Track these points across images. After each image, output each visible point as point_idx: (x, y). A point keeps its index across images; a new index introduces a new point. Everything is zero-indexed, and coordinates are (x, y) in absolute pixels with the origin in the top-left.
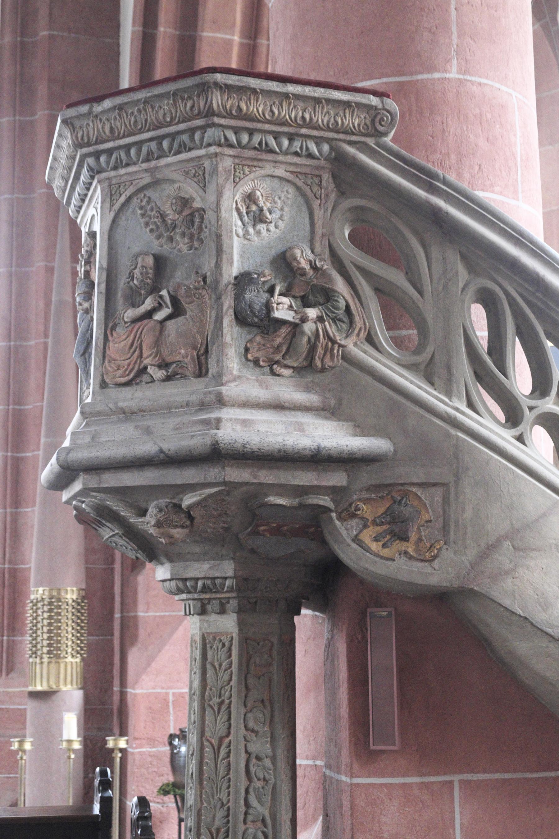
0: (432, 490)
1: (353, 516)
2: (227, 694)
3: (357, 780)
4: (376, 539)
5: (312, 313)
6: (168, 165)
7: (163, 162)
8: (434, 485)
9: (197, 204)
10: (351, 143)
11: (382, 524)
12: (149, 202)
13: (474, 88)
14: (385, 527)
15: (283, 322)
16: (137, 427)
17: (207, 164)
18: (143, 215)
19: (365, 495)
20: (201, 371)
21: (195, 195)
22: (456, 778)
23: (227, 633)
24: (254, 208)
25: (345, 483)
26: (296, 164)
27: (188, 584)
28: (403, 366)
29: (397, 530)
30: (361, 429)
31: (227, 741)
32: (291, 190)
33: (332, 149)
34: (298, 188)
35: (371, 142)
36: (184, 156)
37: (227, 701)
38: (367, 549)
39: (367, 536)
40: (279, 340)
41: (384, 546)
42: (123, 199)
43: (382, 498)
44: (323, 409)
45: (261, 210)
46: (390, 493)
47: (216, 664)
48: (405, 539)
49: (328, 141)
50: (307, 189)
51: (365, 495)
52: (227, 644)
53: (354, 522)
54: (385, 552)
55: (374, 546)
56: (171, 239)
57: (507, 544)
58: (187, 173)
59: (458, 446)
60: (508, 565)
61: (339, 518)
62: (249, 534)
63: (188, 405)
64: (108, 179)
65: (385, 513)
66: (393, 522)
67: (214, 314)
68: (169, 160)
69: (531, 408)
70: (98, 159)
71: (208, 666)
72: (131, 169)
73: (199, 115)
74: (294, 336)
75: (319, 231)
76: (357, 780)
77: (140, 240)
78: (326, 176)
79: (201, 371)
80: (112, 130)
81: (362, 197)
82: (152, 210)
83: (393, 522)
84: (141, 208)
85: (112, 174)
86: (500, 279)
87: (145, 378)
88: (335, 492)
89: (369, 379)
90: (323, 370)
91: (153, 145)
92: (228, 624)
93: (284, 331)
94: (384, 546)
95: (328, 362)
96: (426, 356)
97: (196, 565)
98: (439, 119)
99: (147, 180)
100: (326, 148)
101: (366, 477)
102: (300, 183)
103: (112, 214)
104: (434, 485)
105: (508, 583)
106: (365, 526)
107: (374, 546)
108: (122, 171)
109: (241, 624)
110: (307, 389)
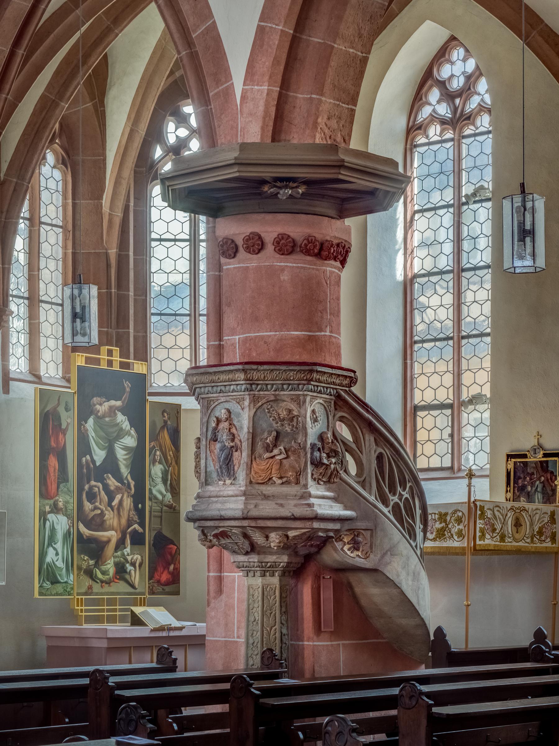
0: (367, 531)
1: (341, 540)
2: (274, 609)
3: (315, 643)
4: (349, 550)
5: (334, 460)
6: (284, 395)
7: (282, 393)
8: (368, 530)
9: (295, 413)
10: (341, 390)
11: (351, 544)
12: (271, 407)
13: (334, 340)
14: (352, 545)
15: (324, 464)
16: (276, 504)
17: (301, 398)
18: (269, 412)
19: (346, 533)
20: (297, 482)
21: (294, 408)
22: (341, 642)
23: (274, 584)
24: (315, 416)
25: (339, 528)
26: (326, 398)
27: (263, 564)
28: (356, 482)
29: (356, 546)
30: (346, 508)
31: (274, 628)
32: (323, 408)
33: (337, 392)
34: (325, 407)
35: (347, 389)
36: (292, 393)
37: (274, 612)
38: (346, 554)
39: (346, 548)
40: (321, 471)
41: (351, 552)
42: (260, 404)
43: (351, 534)
44: (333, 499)
45: (317, 417)
46: (353, 532)
47: (269, 597)
48: (358, 550)
49: (336, 389)
50: (327, 407)
51: (346, 533)
52: (274, 589)
53: (341, 543)
54: (352, 555)
55: (349, 553)
56: (283, 425)
57: (389, 553)
58: (292, 399)
59: (376, 516)
60: (389, 561)
61: (336, 541)
62: (302, 546)
63: (295, 496)
64: (255, 394)
65: (351, 540)
66: (354, 543)
67: (304, 460)
68: (285, 393)
69: (392, 500)
70: (251, 386)
71: (265, 598)
72: (266, 393)
73: (306, 380)
74: (327, 469)
75: (330, 425)
76: (315, 643)
77: (268, 423)
78: (333, 403)
79: (297, 482)
80: (265, 377)
81: (343, 412)
82: (273, 411)
83: (354, 543)
84: (268, 409)
85: (256, 393)
86: (386, 449)
87: (271, 481)
88: (337, 531)
89: (348, 487)
90: (334, 482)
91: (280, 386)
92: (275, 581)
93: (324, 467)
94: (351, 552)
95: (335, 480)
96: (363, 478)
97: (270, 556)
98: (323, 354)
99: (272, 398)
100: (335, 391)
101: (347, 526)
102: (325, 405)
103: (255, 410)
104: (368, 530)
105: (389, 567)
106: (345, 545)
107: (349, 553)
108: (262, 393)
109: (280, 580)
110: (328, 490)
